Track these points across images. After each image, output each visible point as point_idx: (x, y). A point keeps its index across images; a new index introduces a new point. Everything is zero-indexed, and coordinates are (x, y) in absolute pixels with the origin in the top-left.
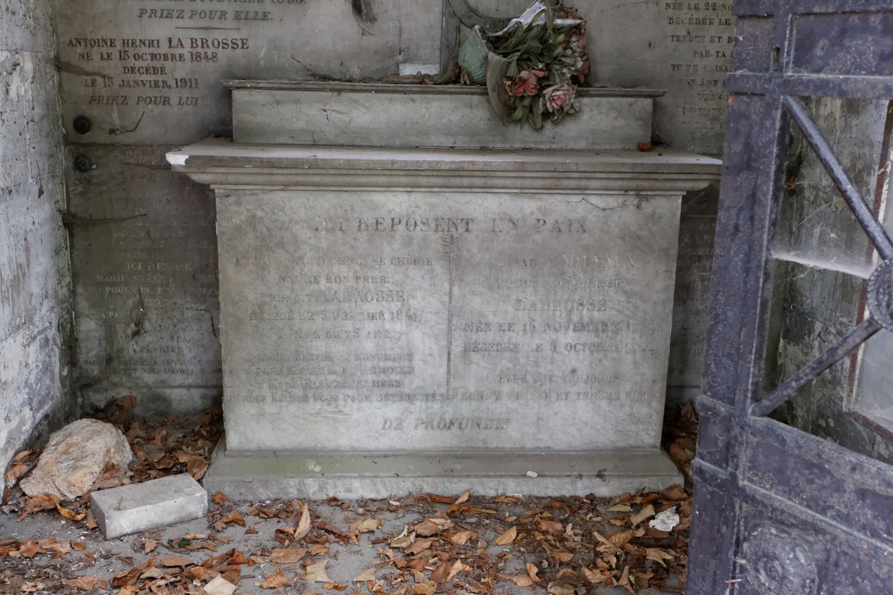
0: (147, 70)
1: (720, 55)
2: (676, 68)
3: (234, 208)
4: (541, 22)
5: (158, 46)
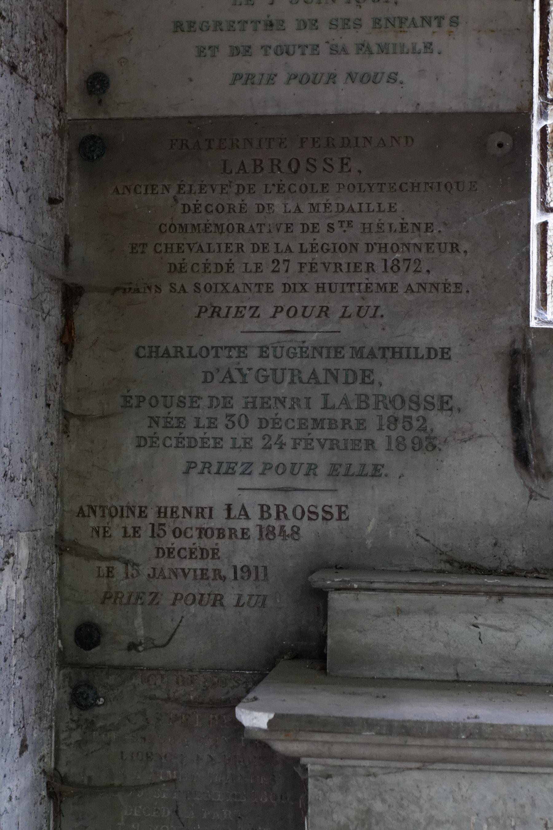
0: (192, 553)
3: (336, 796)
5: (211, 517)
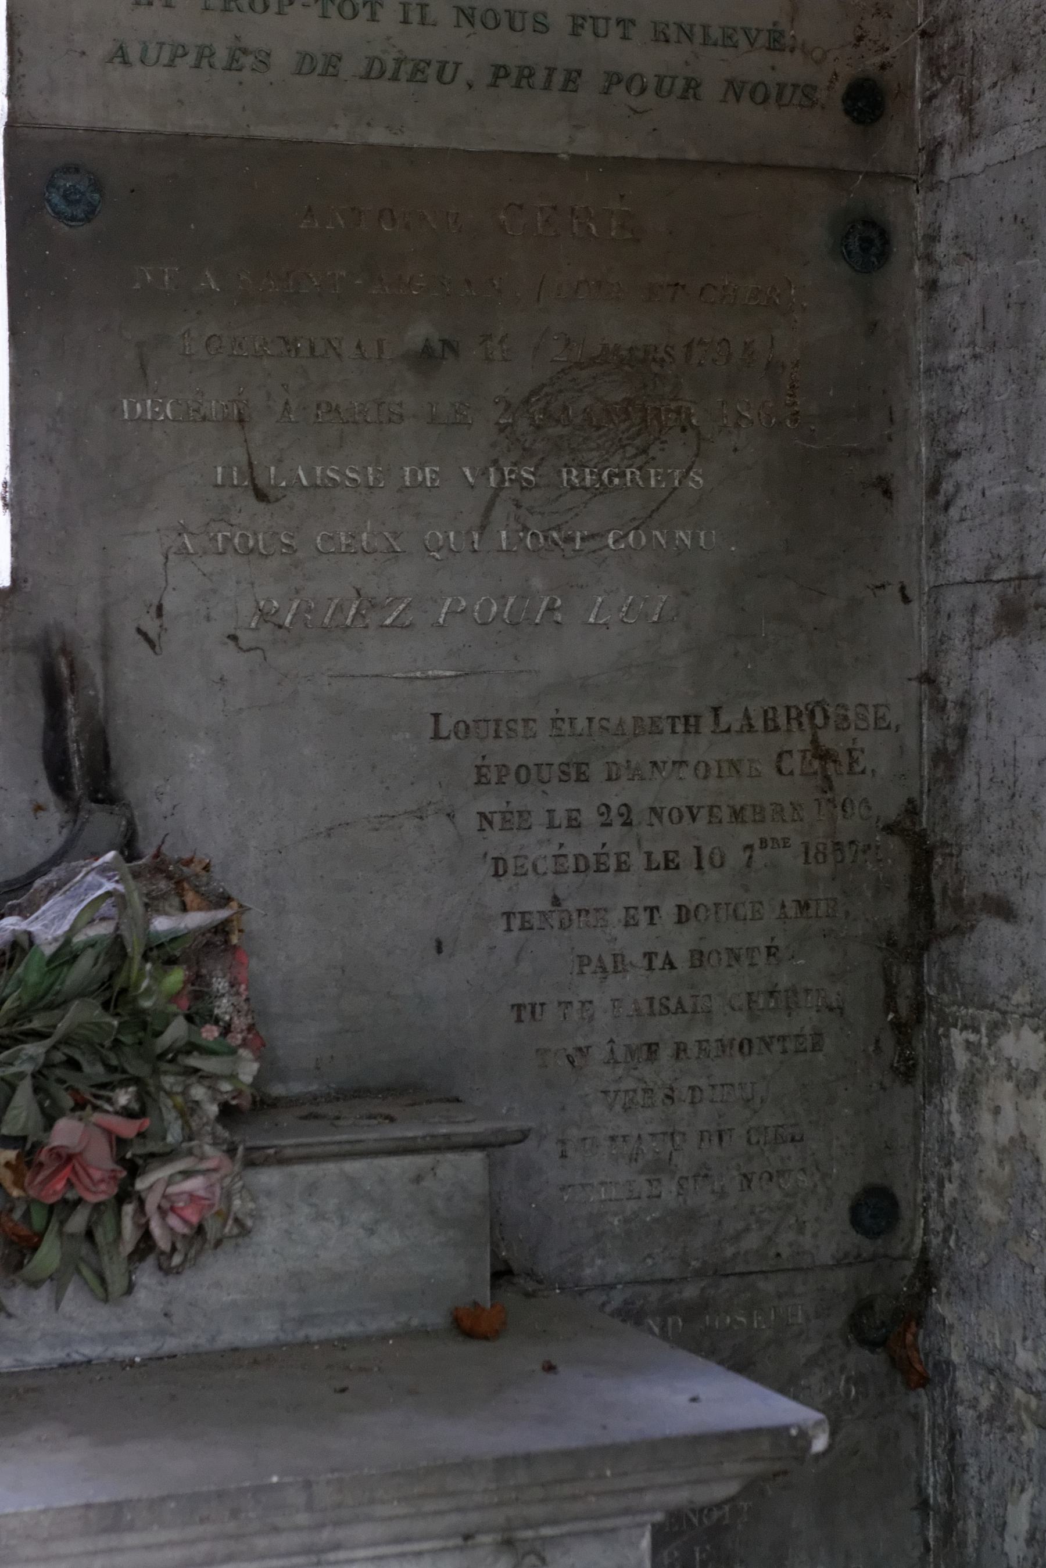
1: (658, 963)
2: (526, 1015)
4: (102, 930)
